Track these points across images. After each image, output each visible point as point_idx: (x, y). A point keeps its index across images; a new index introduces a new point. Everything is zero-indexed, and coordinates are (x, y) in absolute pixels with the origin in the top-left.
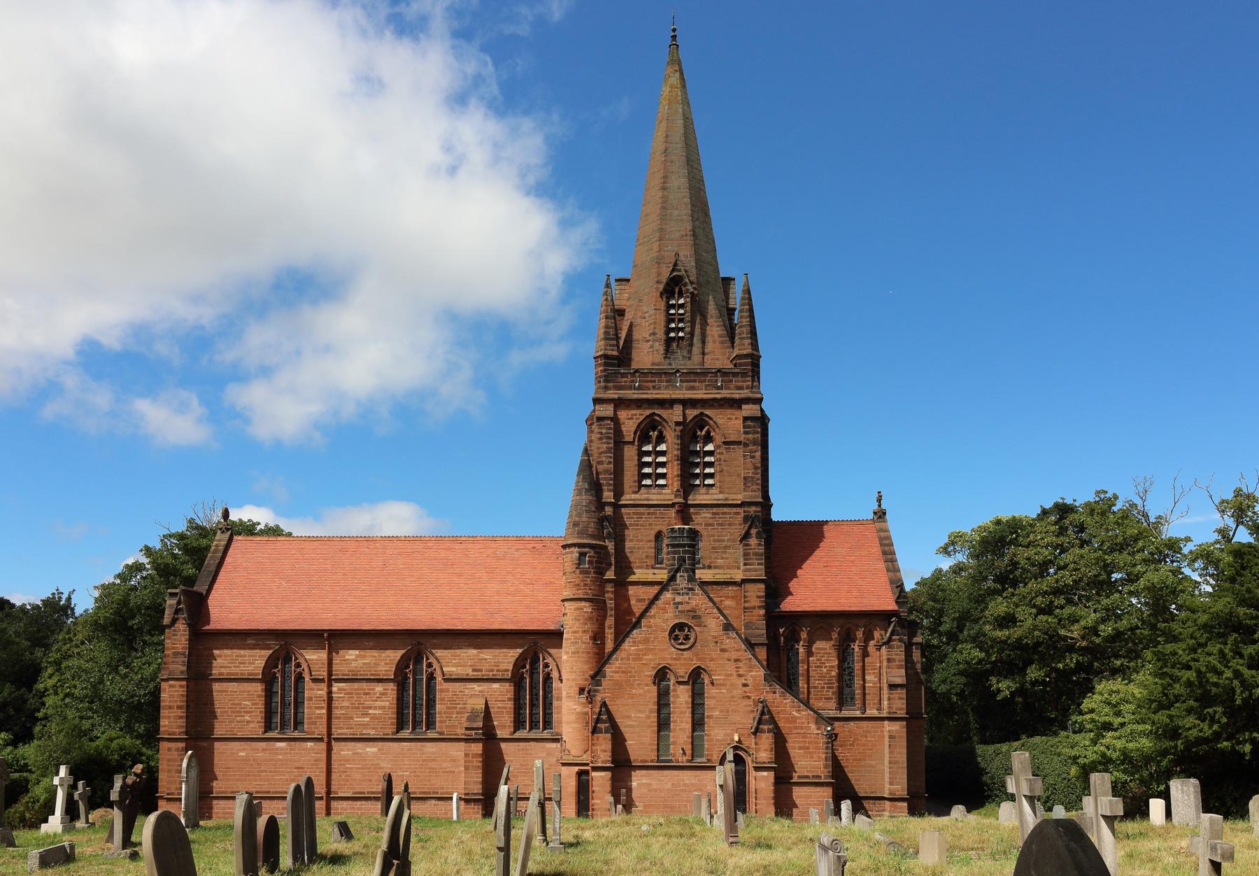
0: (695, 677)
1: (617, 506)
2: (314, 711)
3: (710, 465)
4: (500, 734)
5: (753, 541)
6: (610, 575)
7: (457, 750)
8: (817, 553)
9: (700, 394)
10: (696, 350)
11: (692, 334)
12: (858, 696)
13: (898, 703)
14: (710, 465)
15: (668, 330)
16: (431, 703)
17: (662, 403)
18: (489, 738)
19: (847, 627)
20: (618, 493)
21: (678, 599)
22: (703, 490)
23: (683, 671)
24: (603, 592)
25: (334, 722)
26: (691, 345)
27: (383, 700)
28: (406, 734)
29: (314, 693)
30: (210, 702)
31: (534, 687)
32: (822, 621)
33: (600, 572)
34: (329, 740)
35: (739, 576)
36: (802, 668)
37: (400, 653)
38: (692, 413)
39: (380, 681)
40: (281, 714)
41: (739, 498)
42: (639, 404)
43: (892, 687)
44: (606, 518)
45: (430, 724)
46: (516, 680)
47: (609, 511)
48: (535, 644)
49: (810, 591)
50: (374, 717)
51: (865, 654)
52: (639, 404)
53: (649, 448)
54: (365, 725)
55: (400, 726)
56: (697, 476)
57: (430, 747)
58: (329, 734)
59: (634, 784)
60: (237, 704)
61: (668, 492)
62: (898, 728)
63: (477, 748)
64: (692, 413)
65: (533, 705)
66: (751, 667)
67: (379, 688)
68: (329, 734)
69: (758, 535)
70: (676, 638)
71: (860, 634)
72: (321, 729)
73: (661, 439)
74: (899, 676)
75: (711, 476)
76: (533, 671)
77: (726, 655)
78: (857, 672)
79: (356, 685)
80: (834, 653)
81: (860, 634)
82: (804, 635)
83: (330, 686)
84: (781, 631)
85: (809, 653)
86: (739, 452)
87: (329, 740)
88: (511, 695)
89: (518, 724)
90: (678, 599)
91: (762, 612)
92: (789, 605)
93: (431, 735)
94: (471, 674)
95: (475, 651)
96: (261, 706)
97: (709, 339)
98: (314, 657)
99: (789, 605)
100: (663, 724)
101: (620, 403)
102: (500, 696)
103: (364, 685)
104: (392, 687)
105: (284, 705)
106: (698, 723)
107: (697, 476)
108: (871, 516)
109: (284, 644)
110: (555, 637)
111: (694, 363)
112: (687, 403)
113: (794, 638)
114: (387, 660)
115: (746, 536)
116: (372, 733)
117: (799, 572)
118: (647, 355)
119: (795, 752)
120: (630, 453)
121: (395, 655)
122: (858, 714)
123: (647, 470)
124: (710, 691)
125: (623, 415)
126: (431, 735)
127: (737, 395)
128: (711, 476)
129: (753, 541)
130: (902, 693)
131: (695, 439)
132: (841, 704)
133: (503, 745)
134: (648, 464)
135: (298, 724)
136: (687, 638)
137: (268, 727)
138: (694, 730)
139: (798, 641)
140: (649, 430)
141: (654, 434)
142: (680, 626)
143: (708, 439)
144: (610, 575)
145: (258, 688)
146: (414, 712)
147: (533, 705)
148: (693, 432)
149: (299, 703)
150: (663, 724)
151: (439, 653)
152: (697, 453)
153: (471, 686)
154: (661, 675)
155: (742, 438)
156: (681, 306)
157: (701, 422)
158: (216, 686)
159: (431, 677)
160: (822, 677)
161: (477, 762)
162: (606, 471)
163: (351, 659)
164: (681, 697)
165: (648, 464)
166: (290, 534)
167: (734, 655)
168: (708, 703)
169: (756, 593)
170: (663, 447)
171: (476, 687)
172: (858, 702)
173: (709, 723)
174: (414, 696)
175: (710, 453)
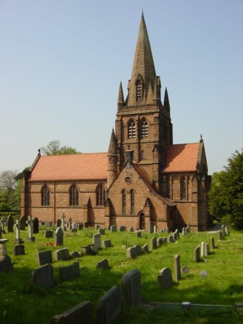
0: (132, 192)
1: (122, 144)
2: (52, 200)
3: (147, 131)
4: (93, 206)
5: (155, 152)
6: (118, 163)
7: (82, 210)
8: (181, 154)
9: (144, 112)
10: (144, 99)
11: (143, 95)
12: (186, 196)
13: (195, 198)
14: (147, 131)
15: (137, 94)
16: (77, 198)
17: (134, 115)
18: (89, 206)
19: (182, 176)
20: (122, 140)
21: (128, 170)
22: (145, 138)
23: (128, 189)
24: (117, 168)
25: (56, 203)
26: (143, 98)
27: (66, 198)
28: (71, 206)
29: (52, 196)
30: (30, 198)
31: (101, 194)
32: (175, 174)
33: (115, 163)
34: (55, 208)
35: (152, 163)
36: (171, 188)
37: (70, 185)
38: (141, 117)
39: (66, 193)
40: (45, 201)
41: (153, 140)
42: (128, 116)
43: (193, 193)
44: (118, 148)
45: (77, 204)
46: (97, 192)
47: (119, 146)
48: (101, 182)
49: (177, 165)
50: (65, 202)
51: (188, 183)
52: (128, 116)
53: (131, 127)
54: (63, 204)
55: (70, 204)
56: (143, 134)
57: (77, 210)
58: (55, 206)
59: (117, 220)
60: (36, 199)
61: (134, 140)
62: (195, 205)
63: (86, 210)
64: (141, 117)
65: (101, 199)
66: (146, 189)
67: (65, 194)
68: (55, 206)
69: (157, 151)
70: (127, 181)
71: (186, 178)
72: (53, 205)
73: (134, 125)
74: (196, 190)
75: (147, 134)
76: (101, 190)
77: (139, 186)
78: (186, 188)
79: (60, 194)
80: (179, 183)
81: (186, 178)
82: (171, 178)
83: (55, 194)
84: (164, 177)
85: (173, 184)
86: (153, 126)
87: (55, 208)
88: (95, 196)
89: (97, 204)
90: (128, 170)
91: (158, 172)
92: (168, 170)
93: (77, 207)
94: (86, 191)
95: (87, 185)
96: (41, 199)
97: (148, 95)
98: (51, 187)
99: (168, 170)
100: (124, 204)
101: (123, 116)
102: (93, 196)
103: (62, 194)
104: (68, 194)
105: (46, 199)
106: (132, 204)
107: (143, 134)
108: (199, 142)
109: (45, 184)
110: (105, 180)
111: (142, 103)
112: (140, 115)
113: (168, 179)
114: (67, 187)
115: (153, 151)
116: (64, 206)
117: (174, 160)
118: (132, 102)
119: (157, 211)
120: (126, 129)
121: (69, 186)
122: (186, 201)
123: (131, 134)
124: (136, 195)
125: (124, 119)
126: (77, 207)
127: (153, 111)
128: (147, 134)
129: (155, 152)
130: (196, 195)
131: (143, 124)
132: (182, 198)
133: (94, 210)
134: (131, 132)
135: (48, 204)
136: (130, 181)
137: (42, 204)
138: (131, 206)
139: (169, 180)
140: (130, 123)
141: (132, 124)
142: (128, 178)
143: (146, 124)
144: (118, 163)
145: (40, 195)
146: (73, 201)
147: (101, 199)
148: (142, 122)
149: (48, 199)
150: (124, 204)
151: (79, 185)
152: (143, 128)
153: (87, 194)
154: (123, 191)
155: (154, 123)
156: (140, 87)
157: (144, 119)
158: (32, 194)
159: (77, 192)
160: (176, 190)
161: (86, 214)
162: (119, 135)
163: (60, 187)
164: (128, 197)
165: (131, 132)
166: (80, 153)
167: (142, 185)
168: (135, 199)
169: (156, 167)
170: (135, 127)
171: (87, 194)
172: (186, 198)
173: (135, 204)
174: (104, 197)
175: (147, 128)
